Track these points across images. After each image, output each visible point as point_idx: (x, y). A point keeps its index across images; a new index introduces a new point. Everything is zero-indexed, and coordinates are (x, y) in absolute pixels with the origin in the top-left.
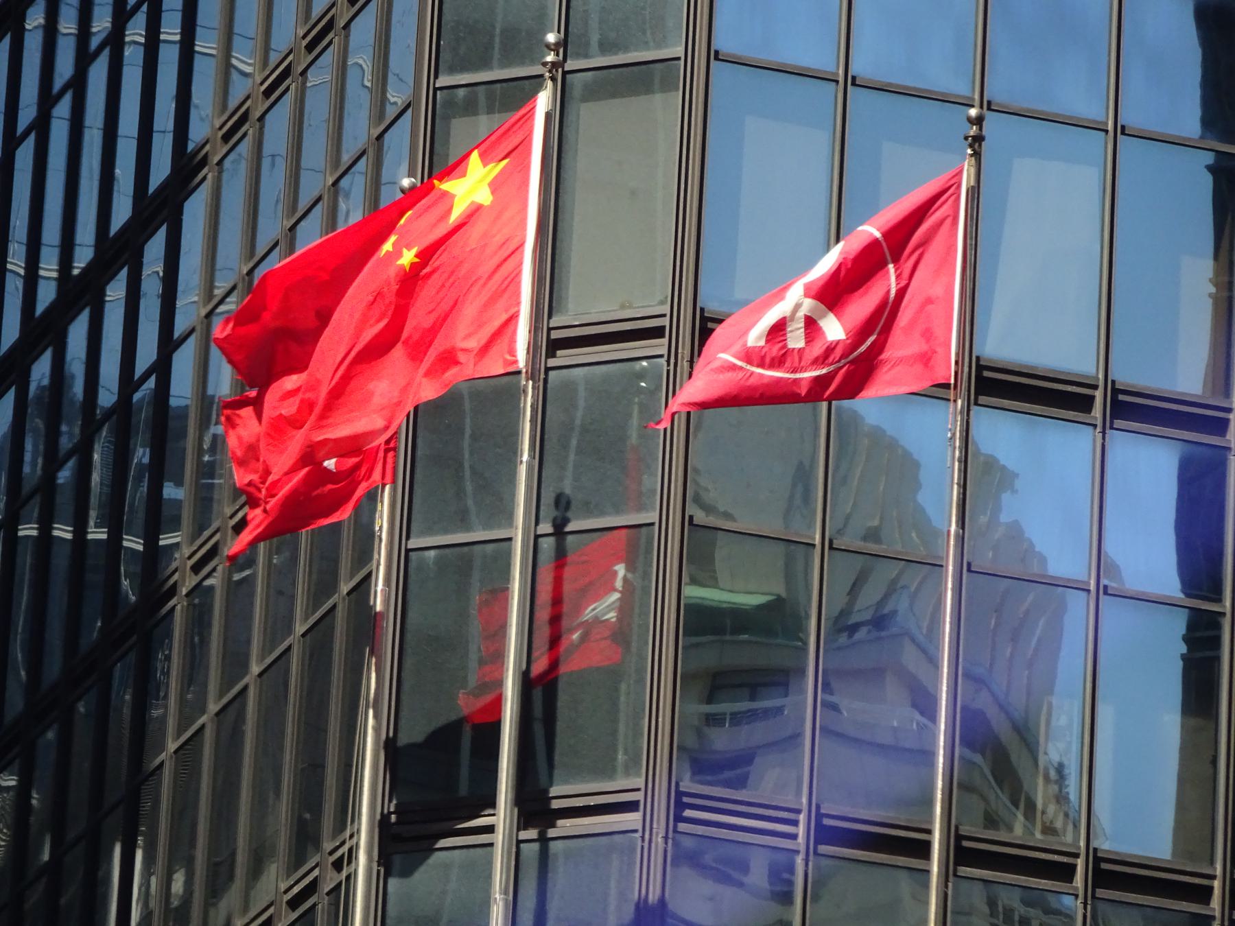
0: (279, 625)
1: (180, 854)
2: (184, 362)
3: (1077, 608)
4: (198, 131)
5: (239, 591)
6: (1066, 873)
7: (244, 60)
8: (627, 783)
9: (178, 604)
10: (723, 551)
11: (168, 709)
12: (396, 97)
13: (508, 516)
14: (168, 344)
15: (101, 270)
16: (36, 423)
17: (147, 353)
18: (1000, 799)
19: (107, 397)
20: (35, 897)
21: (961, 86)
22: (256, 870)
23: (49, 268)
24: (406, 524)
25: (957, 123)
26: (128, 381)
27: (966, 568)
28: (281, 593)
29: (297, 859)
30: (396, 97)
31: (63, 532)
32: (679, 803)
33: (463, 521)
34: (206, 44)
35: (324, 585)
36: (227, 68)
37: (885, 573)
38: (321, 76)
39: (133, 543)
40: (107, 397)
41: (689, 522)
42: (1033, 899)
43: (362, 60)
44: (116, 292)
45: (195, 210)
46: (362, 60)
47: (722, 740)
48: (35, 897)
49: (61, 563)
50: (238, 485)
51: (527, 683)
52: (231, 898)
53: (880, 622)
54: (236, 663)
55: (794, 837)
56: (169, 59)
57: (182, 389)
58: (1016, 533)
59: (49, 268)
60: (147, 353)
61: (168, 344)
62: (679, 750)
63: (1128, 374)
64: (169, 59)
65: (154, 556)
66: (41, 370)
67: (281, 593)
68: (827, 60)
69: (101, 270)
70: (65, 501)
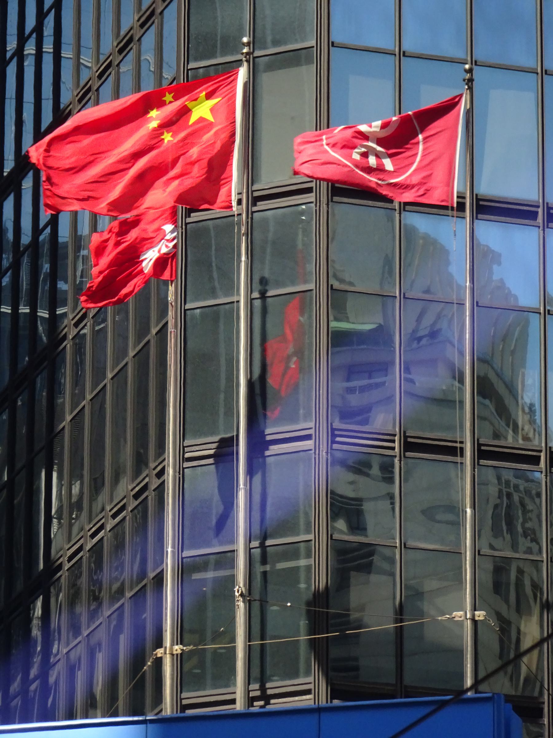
0: (120, 353)
3: (535, 322)
4: (66, 97)
5: (100, 336)
6: (535, 460)
7: (87, 60)
9: (68, 345)
10: (351, 303)
18: (501, 424)
19: (26, 239)
21: (460, 53)
22: (116, 479)
26: (36, 230)
27: (475, 304)
29: (137, 472)
32: (333, 434)
33: (213, 294)
34: (67, 53)
36: (78, 65)
39: (43, 314)
40: (26, 239)
43: (149, 56)
46: (149, 56)
47: (355, 400)
51: (250, 384)
52: (104, 496)
53: (433, 334)
58: (502, 283)
62: (331, 407)
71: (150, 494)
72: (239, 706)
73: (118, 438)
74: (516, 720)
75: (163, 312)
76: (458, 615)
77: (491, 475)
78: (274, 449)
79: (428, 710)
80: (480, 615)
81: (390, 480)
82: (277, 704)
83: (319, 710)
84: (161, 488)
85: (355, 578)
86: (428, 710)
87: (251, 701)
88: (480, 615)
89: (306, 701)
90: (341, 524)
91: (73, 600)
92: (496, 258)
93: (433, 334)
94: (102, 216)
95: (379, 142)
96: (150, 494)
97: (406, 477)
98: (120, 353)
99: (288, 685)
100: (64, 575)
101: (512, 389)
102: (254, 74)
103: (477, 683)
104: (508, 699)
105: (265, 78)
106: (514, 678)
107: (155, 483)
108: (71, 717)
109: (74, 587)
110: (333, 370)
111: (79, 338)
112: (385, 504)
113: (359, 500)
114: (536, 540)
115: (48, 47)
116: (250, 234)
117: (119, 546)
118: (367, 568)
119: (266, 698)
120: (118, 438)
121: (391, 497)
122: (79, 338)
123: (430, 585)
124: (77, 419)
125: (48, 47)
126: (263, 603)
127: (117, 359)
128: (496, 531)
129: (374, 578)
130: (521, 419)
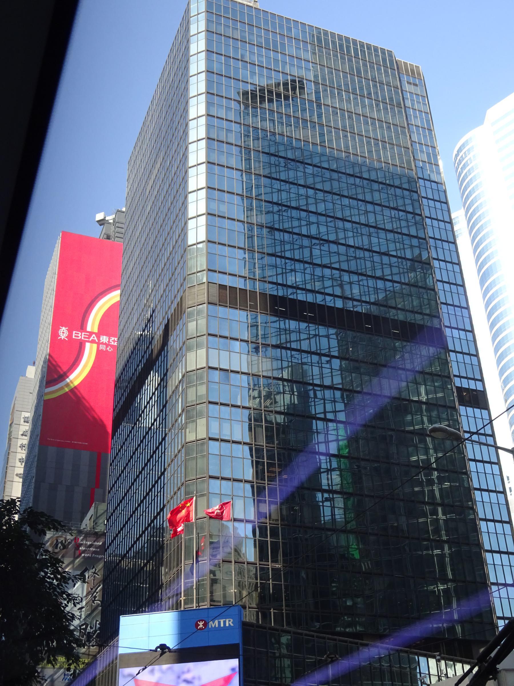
0: (174, 546)
1: (166, 567)
2: (165, 523)
3: (244, 539)
4: (165, 502)
5: (170, 543)
6: (244, 563)
7: (169, 496)
8: (205, 558)
9: (165, 545)
10: (213, 536)
11: (165, 554)
12: (182, 498)
13: (193, 534)
14: (163, 522)
15: (157, 515)
16: (152, 529)
17: (161, 523)
18: (239, 557)
19: (158, 527)
20: (154, 572)
21: (231, 494)
22: (173, 568)
23: (153, 515)
24: (185, 536)
25: (231, 497)
26: (160, 525)
27: (234, 536)
28: (174, 543)
29: (177, 567)
30: (182, 498)
31: (155, 539)
32: (210, 559)
33: (190, 536)
34: (165, 495)
35: (178, 542)
36: (167, 497)
37: (227, 538)
38: (175, 497)
39: (161, 539)
40: (158, 527)
41: (210, 534)
42: (242, 566)
43: (179, 495)
44: (158, 517)
45: (165, 510)
46: (179, 495)
47: (214, 553)
48: (154, 572)
49: (152, 542)
50: (21, 378)
51: (196, 551)
52: (171, 571)
53: (227, 541)
54: (170, 550)
55: (269, 565)
56: (162, 496)
57: (165, 526)
58: (238, 533)
59: (153, 515)
60: (161, 523)
61: (163, 522)
62: (210, 555)
63: (247, 518)
64: (162, 496)
65: (163, 541)
66: (152, 525)
67: (174, 543)
68: (219, 492)
69: (157, 515)
70: (155, 536)
71: (179, 571)
72: (195, 608)
73: (174, 560)
74: (242, 609)
75: (181, 539)
76: (232, 591)
77: (237, 566)
78: (200, 562)
79: (227, 608)
80: (236, 591)
81: (220, 567)
82: (201, 607)
83: (208, 608)
84: (181, 570)
85: (214, 585)
86: (227, 608)
87: (197, 607)
88: (236, 591)
89: (206, 607)
90: (212, 575)
91: (166, 589)
92: (237, 528)
93: (227, 541)
94: (232, 375)
95: (398, 350)
96: (179, 571)
97: (223, 566)
98: (174, 546)
99: (203, 604)
100: (164, 585)
101: (240, 551)
102: (196, 498)
103: (235, 603)
104: (241, 605)
105: (198, 499)
106: (242, 601)
107: (180, 569)
108: (166, 610)
109: (166, 587)
110: (210, 548)
111: (167, 544)
112: (219, 571)
113: (215, 571)
114: (245, 577)
115: (162, 494)
116: (196, 525)
117: (174, 580)
118: (216, 583)
119: (199, 606)
120: (174, 560)
121: (220, 570)
122: (167, 544)
123: (227, 585)
124: (167, 558)
125: (162, 494)
126: (198, 589)
127: (166, 555)
128: (238, 575)
129: (218, 584)
130: (242, 556)
